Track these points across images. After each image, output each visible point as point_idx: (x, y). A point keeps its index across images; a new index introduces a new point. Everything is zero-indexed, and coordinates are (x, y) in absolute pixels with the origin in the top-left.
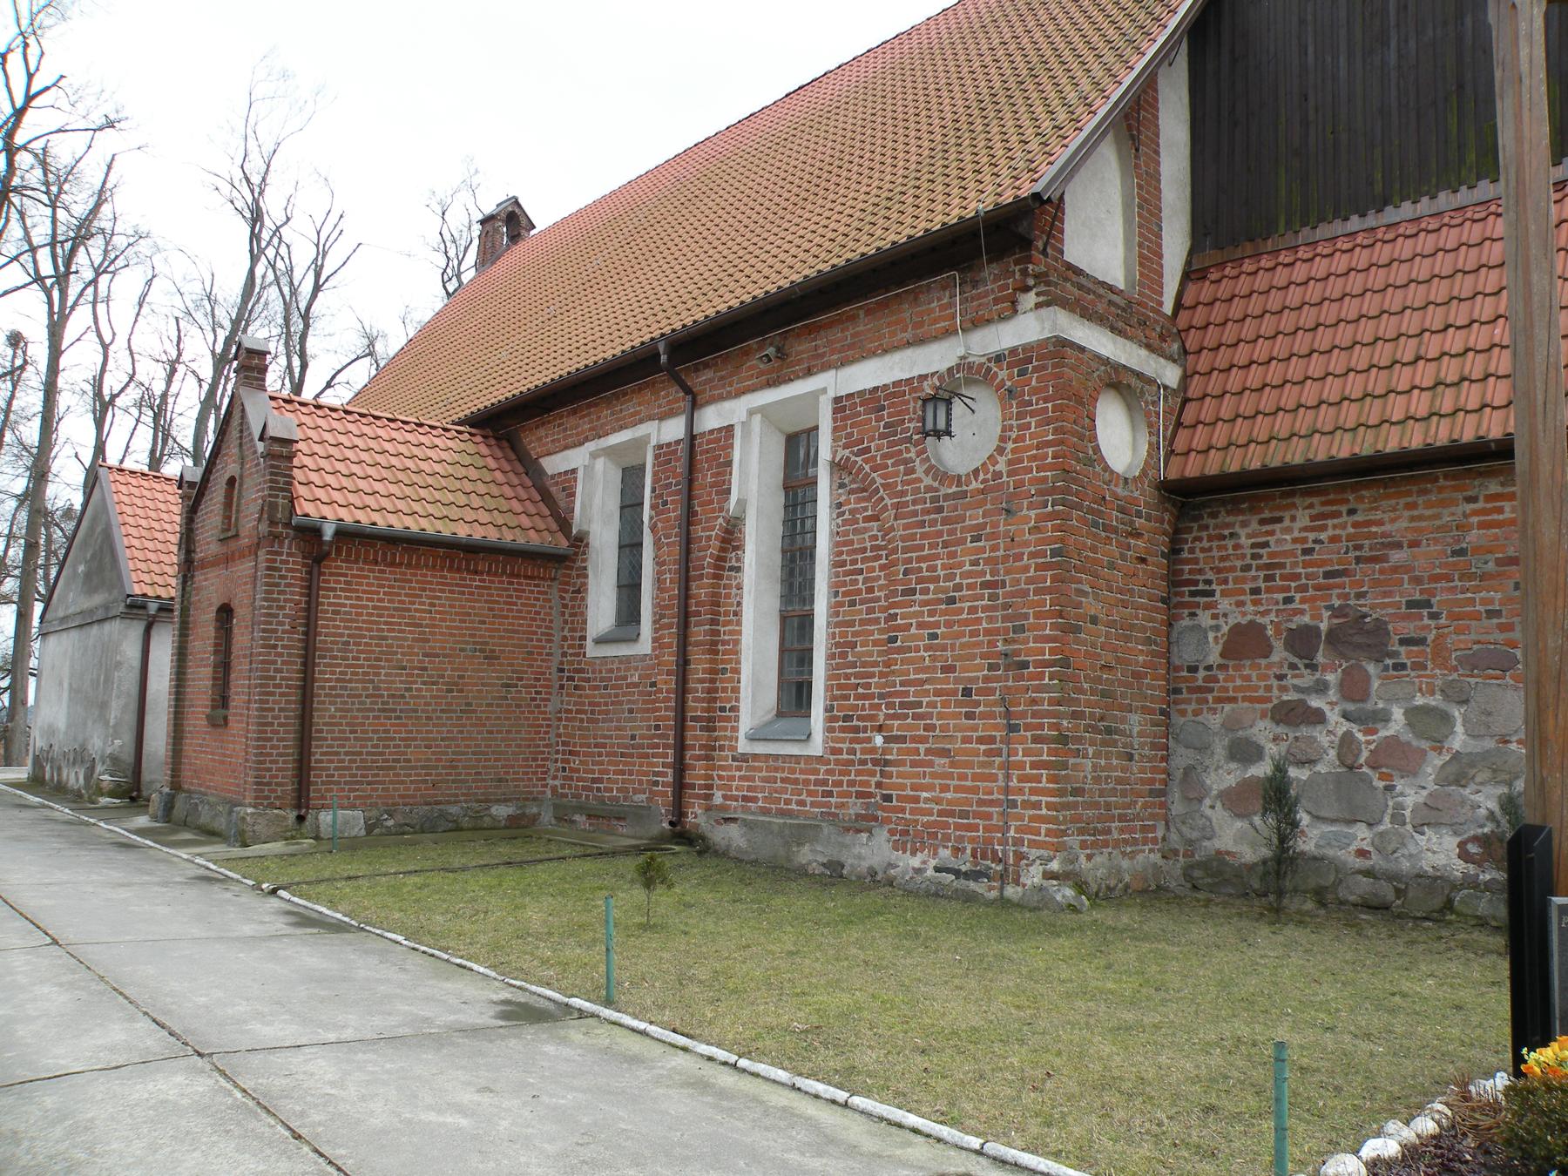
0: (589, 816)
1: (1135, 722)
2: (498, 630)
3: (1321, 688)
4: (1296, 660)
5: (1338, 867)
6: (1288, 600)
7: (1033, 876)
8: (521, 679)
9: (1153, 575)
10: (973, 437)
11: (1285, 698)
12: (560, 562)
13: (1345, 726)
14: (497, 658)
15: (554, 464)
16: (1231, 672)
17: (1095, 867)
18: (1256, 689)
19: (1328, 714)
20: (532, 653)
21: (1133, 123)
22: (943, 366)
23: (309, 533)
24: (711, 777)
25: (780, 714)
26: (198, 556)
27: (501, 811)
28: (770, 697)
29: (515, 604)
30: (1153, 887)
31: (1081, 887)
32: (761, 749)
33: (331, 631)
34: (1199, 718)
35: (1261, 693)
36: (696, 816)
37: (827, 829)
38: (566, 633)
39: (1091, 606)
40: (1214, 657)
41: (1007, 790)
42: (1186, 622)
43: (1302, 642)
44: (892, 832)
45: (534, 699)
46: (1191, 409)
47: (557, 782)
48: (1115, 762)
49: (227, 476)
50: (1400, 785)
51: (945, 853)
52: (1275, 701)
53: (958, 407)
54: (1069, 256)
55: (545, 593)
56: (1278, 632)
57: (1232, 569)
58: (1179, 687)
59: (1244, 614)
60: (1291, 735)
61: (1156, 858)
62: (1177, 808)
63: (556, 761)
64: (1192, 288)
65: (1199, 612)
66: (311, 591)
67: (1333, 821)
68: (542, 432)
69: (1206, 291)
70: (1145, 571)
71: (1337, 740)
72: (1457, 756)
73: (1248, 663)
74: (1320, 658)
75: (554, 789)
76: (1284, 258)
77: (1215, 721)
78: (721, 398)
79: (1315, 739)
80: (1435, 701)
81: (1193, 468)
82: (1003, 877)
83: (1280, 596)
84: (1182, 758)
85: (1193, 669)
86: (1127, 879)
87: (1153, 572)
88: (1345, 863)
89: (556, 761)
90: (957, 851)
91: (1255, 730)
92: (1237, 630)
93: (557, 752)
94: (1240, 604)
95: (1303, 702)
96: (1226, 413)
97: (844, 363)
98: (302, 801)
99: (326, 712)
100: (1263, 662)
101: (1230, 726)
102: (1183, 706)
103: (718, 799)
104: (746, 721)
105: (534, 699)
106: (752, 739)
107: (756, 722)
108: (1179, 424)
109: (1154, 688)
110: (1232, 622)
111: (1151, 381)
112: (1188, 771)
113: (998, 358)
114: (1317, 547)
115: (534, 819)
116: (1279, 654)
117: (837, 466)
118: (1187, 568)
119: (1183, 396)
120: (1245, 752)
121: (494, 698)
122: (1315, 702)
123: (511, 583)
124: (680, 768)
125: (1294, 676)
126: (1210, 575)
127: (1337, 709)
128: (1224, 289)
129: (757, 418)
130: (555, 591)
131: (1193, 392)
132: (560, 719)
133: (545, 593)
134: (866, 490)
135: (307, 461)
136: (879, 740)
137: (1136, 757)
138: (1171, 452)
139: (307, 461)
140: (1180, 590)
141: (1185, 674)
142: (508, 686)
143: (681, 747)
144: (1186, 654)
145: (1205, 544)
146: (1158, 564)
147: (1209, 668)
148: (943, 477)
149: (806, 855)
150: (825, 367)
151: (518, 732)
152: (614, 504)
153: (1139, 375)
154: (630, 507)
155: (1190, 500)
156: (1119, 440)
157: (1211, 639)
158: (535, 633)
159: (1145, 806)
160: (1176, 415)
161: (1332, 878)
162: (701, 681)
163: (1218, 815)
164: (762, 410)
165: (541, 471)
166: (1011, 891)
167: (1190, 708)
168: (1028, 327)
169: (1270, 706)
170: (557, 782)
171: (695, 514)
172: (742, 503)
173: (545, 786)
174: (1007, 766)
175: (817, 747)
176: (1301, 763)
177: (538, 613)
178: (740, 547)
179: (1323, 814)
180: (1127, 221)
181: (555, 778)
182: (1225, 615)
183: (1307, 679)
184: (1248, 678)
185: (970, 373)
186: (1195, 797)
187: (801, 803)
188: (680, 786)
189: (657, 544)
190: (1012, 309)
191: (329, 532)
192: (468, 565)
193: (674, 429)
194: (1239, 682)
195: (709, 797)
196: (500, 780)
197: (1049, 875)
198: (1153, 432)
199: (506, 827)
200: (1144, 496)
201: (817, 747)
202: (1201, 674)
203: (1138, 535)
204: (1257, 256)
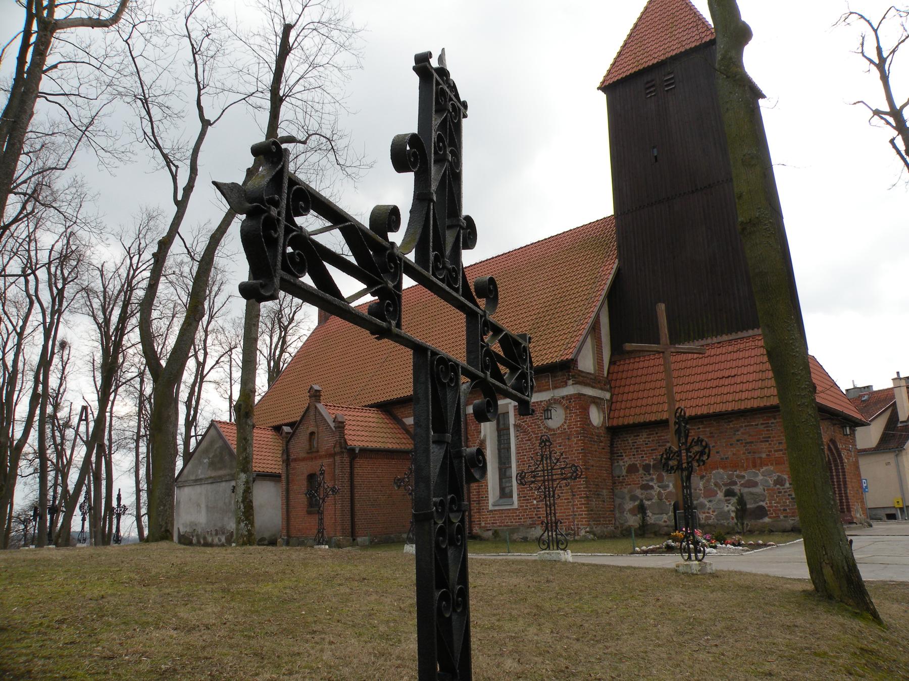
1: (605, 492)
3: (652, 480)
7: (583, 533)
13: (659, 489)
17: (598, 530)
21: (595, 328)
22: (547, 399)
23: (352, 450)
25: (501, 498)
26: (292, 457)
31: (595, 535)
32: (497, 508)
33: (357, 480)
37: (521, 528)
39: (591, 462)
40: (624, 473)
43: (647, 468)
46: (614, 405)
49: (309, 431)
58: (616, 482)
61: (613, 528)
62: (618, 515)
64: (612, 367)
66: (352, 467)
68: (402, 410)
69: (616, 368)
76: (637, 360)
77: (626, 491)
81: (615, 423)
82: (574, 534)
84: (618, 501)
92: (630, 466)
96: (623, 407)
98: (353, 535)
99: (358, 506)
103: (483, 524)
104: (491, 501)
108: (611, 410)
111: (603, 399)
112: (620, 505)
113: (563, 398)
116: (641, 471)
119: (611, 401)
120: (633, 498)
122: (651, 484)
128: (621, 368)
131: (614, 400)
134: (525, 432)
136: (535, 502)
138: (609, 418)
140: (613, 455)
144: (617, 472)
146: (608, 449)
148: (550, 429)
149: (515, 536)
153: (599, 398)
155: (615, 432)
156: (596, 417)
160: (610, 407)
163: (628, 516)
165: (404, 423)
166: (577, 538)
168: (570, 390)
172: (485, 436)
174: (573, 505)
175: (516, 505)
176: (648, 500)
180: (593, 353)
183: (649, 478)
186: (622, 512)
190: (566, 385)
197: (586, 532)
200: (602, 431)
201: (516, 505)
204: (629, 359)
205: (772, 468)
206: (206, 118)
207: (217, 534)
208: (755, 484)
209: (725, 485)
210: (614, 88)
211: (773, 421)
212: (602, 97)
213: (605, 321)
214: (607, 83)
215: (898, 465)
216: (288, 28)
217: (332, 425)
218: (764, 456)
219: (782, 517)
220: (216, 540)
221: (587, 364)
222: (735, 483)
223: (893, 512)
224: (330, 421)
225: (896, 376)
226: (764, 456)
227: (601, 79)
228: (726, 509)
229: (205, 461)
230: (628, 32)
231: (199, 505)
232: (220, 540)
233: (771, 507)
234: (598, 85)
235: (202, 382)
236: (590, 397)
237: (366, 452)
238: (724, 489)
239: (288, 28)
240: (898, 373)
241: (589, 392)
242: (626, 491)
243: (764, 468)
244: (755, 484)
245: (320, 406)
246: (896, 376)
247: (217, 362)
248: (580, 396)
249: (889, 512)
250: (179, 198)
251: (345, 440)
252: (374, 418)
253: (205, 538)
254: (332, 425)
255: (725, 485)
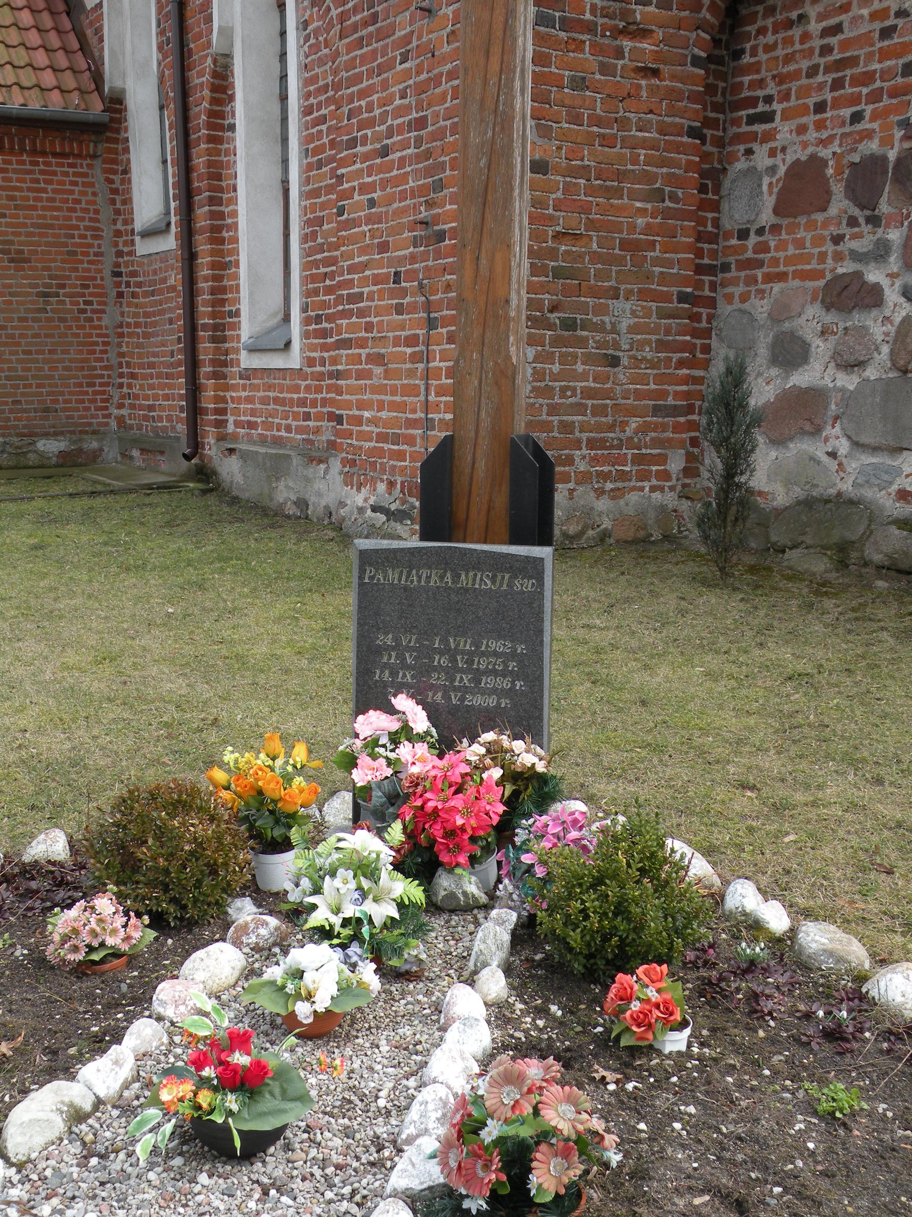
0: (143, 451)
2: (24, 225)
3: (880, 253)
4: (856, 212)
5: (872, 516)
6: (857, 117)
8: (63, 286)
9: (673, 95)
11: (840, 271)
14: (28, 261)
16: (784, 236)
18: (807, 258)
19: (887, 291)
20: (74, 253)
24: (224, 400)
27: (51, 447)
29: (44, 191)
30: (656, 535)
34: (746, 306)
35: (814, 265)
38: (119, 226)
40: (766, 217)
42: (741, 165)
44: (344, 462)
45: (84, 311)
47: (124, 412)
48: (580, 367)
52: (829, 276)
55: (85, 175)
56: (839, 171)
57: (796, 75)
59: (805, 145)
60: (841, 325)
63: (121, 386)
65: (755, 147)
67: (875, 449)
70: (652, 90)
71: (893, 330)
73: (802, 220)
74: (884, 207)
75: (121, 420)
79: (865, 328)
83: (846, 112)
85: (743, 234)
86: (607, 524)
87: (673, 90)
88: (881, 509)
89: (121, 386)
91: (802, 321)
93: (121, 375)
94: (802, 130)
95: (858, 275)
100: (819, 217)
101: (779, 315)
102: (730, 290)
105: (84, 311)
107: (257, 329)
109: (671, 264)
110: (790, 158)
114: (900, 22)
115: (95, 456)
116: (839, 204)
118: (746, 79)
121: (27, 310)
122: (874, 276)
123: (37, 164)
124: (194, 390)
125: (854, 237)
126: (771, 89)
127: (898, 283)
130: (98, 171)
132: (121, 335)
133: (85, 175)
137: (625, 361)
141: (734, 242)
142: (46, 295)
143: (193, 364)
144: (735, 213)
145: (770, 38)
147: (760, 231)
151: (67, 352)
157: (765, 188)
158: (77, 228)
159: (644, 429)
161: (861, 529)
162: (206, 279)
167: (737, 291)
169: (821, 283)
170: (124, 412)
171: (190, 50)
173: (109, 416)
175: (294, 360)
177: (78, 202)
179: (864, 439)
181: (121, 406)
182: (784, 149)
184: (800, 244)
187: (288, 429)
188: (195, 411)
192: (22, 143)
194: (791, 250)
196: (46, 410)
199: (57, 466)
202: (753, 239)
203: (643, 33)
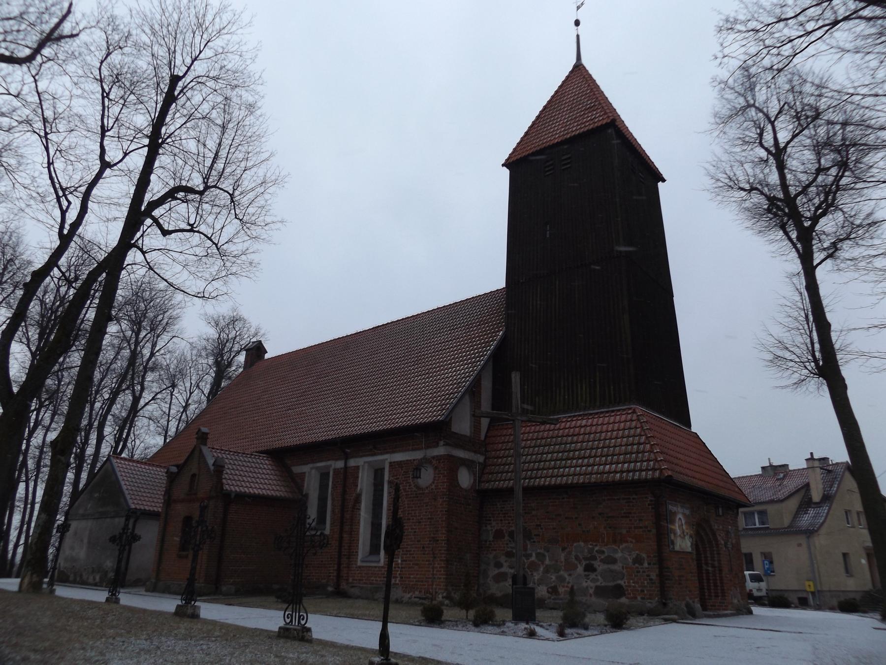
10: (427, 477)
12: (301, 503)
15: (297, 469)
22: (419, 457)
27: (276, 587)
28: (368, 548)
32: (364, 564)
36: (344, 586)
40: (491, 538)
41: (433, 574)
50: (535, 574)
51: (417, 593)
53: (423, 470)
54: (453, 430)
72: (547, 566)
77: (491, 556)
78: (356, 457)
80: (542, 551)
85: (486, 541)
90: (420, 592)
97: (393, 452)
103: (350, 580)
106: (362, 561)
113: (433, 458)
116: (507, 538)
117: (390, 482)
119: (484, 465)
124: (339, 570)
129: (366, 465)
135: (228, 471)
138: (479, 481)
139: (228, 471)
143: (339, 564)
148: (418, 487)
150: (387, 453)
152: (317, 485)
154: (323, 487)
156: (465, 479)
164: (369, 463)
168: (441, 451)
172: (361, 490)
174: (433, 568)
178: (360, 503)
185: (426, 461)
189: (333, 500)
190: (437, 445)
191: (233, 495)
193: (340, 464)
195: (347, 580)
198: (475, 475)
201: (382, 563)
205: (631, 546)
206: (107, 159)
207: (93, 572)
208: (614, 561)
209: (586, 559)
210: (516, 164)
211: (634, 496)
212: (506, 172)
213: (487, 385)
214: (511, 161)
215: (809, 547)
216: (175, 80)
217: (212, 468)
218: (624, 531)
219: (639, 598)
220: (91, 580)
221: (463, 426)
222: (595, 558)
223: (804, 595)
224: (211, 462)
225: (809, 457)
226: (624, 531)
227: (507, 157)
228: (585, 584)
229: (96, 495)
230: (537, 113)
231: (82, 541)
232: (94, 579)
233: (630, 586)
234: (503, 162)
235: (135, 416)
236: (461, 459)
237: (241, 497)
238: (584, 563)
239: (175, 80)
240: (812, 454)
241: (461, 454)
242: (491, 556)
243: (624, 545)
244: (614, 561)
245: (205, 450)
246: (809, 457)
247: (153, 399)
248: (450, 457)
249: (801, 595)
250: (65, 232)
251: (222, 484)
252: (266, 465)
253: (81, 576)
254: (212, 468)
255: (586, 559)
